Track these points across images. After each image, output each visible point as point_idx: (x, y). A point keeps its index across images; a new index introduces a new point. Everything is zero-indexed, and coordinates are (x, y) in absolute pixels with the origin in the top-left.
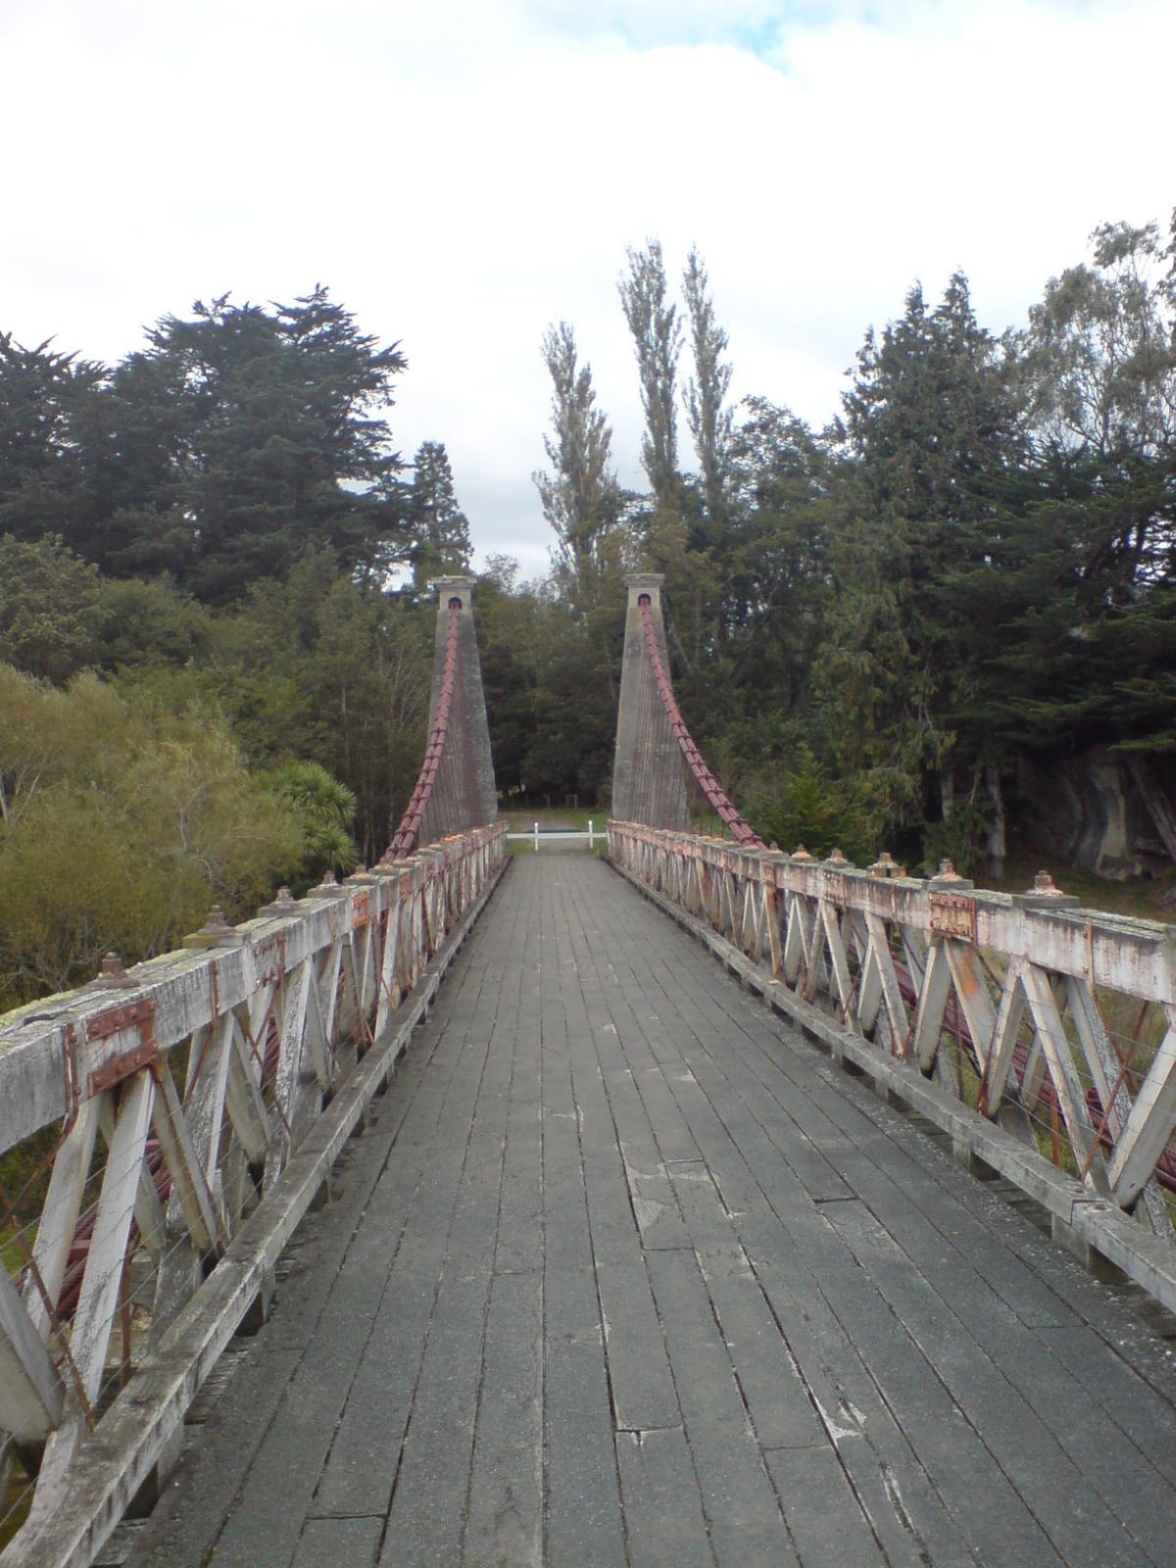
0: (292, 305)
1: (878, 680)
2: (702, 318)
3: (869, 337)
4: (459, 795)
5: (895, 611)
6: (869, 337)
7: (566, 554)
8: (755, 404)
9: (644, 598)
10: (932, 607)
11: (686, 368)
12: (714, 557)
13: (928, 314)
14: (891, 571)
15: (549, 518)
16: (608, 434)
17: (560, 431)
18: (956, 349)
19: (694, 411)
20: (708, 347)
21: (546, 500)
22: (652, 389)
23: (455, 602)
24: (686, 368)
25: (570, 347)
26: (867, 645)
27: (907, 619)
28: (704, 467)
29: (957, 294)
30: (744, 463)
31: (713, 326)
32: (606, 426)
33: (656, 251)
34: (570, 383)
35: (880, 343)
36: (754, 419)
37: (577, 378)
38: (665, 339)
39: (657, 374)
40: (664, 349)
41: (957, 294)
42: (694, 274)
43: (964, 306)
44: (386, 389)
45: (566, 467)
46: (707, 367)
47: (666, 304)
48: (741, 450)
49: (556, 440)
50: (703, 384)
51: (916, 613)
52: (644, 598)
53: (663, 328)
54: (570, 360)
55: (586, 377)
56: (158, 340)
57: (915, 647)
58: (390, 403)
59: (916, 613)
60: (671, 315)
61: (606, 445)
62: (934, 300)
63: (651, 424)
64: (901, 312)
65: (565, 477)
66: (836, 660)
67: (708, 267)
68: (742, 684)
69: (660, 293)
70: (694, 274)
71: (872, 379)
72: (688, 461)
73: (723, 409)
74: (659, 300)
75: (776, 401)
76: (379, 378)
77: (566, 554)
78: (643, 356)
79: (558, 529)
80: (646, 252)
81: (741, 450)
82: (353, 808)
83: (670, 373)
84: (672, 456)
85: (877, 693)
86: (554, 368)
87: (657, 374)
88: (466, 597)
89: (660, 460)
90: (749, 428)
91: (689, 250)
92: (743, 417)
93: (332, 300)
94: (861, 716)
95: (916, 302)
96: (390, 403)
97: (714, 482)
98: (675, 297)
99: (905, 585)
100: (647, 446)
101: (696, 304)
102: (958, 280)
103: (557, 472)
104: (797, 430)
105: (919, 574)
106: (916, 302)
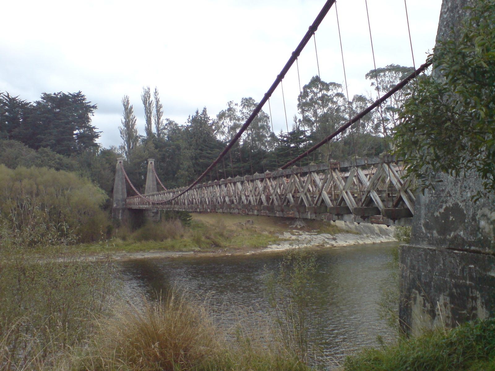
0: (72, 93)
1: (189, 177)
2: (157, 102)
3: (189, 116)
4: (120, 193)
5: (192, 165)
6: (189, 116)
7: (125, 145)
8: (167, 120)
9: (151, 163)
10: (198, 165)
11: (154, 111)
12: (159, 151)
13: (199, 115)
14: (192, 158)
15: (121, 137)
16: (136, 120)
17: (125, 118)
18: (204, 120)
19: (155, 120)
20: (159, 107)
21: (121, 133)
22: (147, 116)
23: (120, 162)
24: (154, 111)
25: (128, 101)
26: (187, 170)
27: (194, 167)
28: (157, 131)
29: (205, 111)
30: (166, 131)
31: (160, 103)
32: (135, 119)
33: (149, 89)
34: (128, 108)
35: (191, 118)
36: (167, 123)
37: (129, 107)
38: (150, 107)
39: (148, 113)
40: (150, 108)
41: (205, 111)
42: (156, 92)
43: (206, 113)
44: (93, 113)
45: (125, 126)
46: (158, 111)
47: (151, 100)
48: (165, 129)
49: (124, 120)
50: (157, 115)
51: (196, 166)
52: (151, 163)
53: (150, 104)
54: (128, 103)
55: (131, 108)
56: (42, 98)
57: (195, 171)
58: (93, 115)
59: (196, 166)
60: (151, 102)
61: (135, 122)
62: (200, 112)
63: (147, 123)
64: (195, 114)
65: (125, 128)
66: (182, 173)
67: (159, 91)
68: (163, 175)
69: (149, 97)
70: (156, 92)
71: (190, 124)
72: (154, 130)
73: (161, 120)
74: (149, 99)
75: (171, 119)
76: (92, 111)
77: (125, 145)
78: (146, 109)
79: (123, 139)
80: (147, 89)
81: (165, 129)
82: (232, 188)
83: (151, 113)
84: (151, 129)
85: (188, 179)
86: (124, 105)
87: (148, 113)
88: (122, 162)
89: (148, 130)
90: (166, 125)
91: (155, 87)
92: (165, 122)
93: (82, 93)
94: (186, 182)
95: (197, 112)
96: (93, 115)
97: (159, 135)
98: (152, 98)
99: (194, 161)
100: (146, 127)
101: (156, 99)
102: (205, 109)
103: (124, 127)
104: (176, 124)
105: (196, 159)
106: (197, 112)
